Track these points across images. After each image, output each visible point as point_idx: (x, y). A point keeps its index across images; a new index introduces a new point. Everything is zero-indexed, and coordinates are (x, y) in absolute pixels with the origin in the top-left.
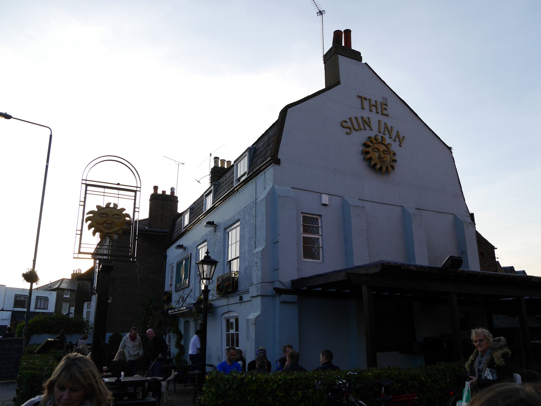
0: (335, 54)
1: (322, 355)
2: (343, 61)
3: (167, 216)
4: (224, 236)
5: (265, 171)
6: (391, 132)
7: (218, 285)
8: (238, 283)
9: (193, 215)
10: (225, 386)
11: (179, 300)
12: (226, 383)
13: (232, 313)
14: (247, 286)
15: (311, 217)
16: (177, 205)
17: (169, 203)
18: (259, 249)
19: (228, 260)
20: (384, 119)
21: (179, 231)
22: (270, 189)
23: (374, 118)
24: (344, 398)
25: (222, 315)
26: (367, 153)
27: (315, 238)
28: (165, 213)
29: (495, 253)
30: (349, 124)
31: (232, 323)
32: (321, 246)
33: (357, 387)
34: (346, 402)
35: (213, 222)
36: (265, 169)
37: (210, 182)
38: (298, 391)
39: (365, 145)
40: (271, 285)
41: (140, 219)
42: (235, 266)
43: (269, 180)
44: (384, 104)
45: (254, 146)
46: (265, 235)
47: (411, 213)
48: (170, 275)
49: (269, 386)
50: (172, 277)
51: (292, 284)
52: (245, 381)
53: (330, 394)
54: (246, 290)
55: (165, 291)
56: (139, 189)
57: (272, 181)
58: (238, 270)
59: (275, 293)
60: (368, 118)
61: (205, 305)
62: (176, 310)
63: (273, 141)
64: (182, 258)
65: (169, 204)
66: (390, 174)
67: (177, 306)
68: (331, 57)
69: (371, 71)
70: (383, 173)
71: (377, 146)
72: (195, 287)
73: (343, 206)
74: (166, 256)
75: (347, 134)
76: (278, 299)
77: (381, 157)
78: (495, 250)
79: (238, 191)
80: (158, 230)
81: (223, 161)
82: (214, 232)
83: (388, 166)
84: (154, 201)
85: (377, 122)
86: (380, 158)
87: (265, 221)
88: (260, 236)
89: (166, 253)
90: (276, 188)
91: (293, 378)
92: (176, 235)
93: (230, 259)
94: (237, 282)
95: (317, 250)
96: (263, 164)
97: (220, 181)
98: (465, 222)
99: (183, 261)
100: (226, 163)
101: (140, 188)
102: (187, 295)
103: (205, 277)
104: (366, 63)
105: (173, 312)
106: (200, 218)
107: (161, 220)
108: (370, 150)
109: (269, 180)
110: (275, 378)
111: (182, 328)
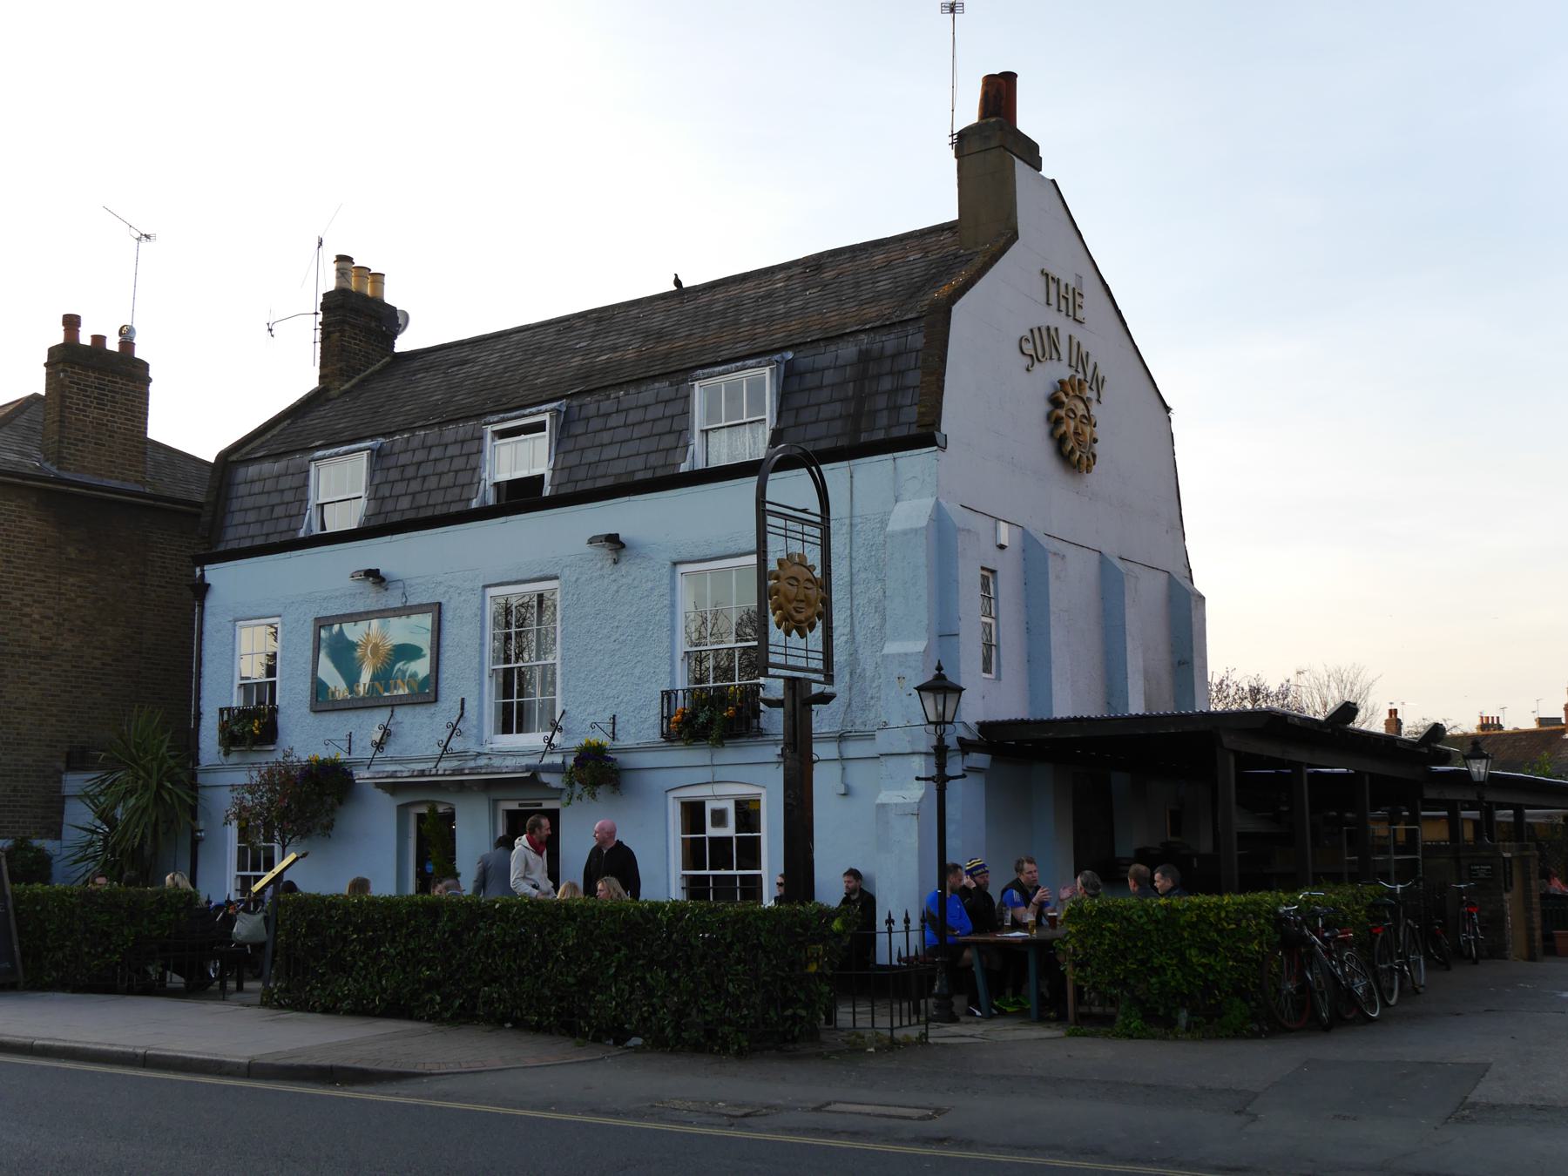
0: (1002, 149)
17: (123, 384)
28: (108, 421)
32: (994, 642)
65: (121, 388)
107: (96, 444)
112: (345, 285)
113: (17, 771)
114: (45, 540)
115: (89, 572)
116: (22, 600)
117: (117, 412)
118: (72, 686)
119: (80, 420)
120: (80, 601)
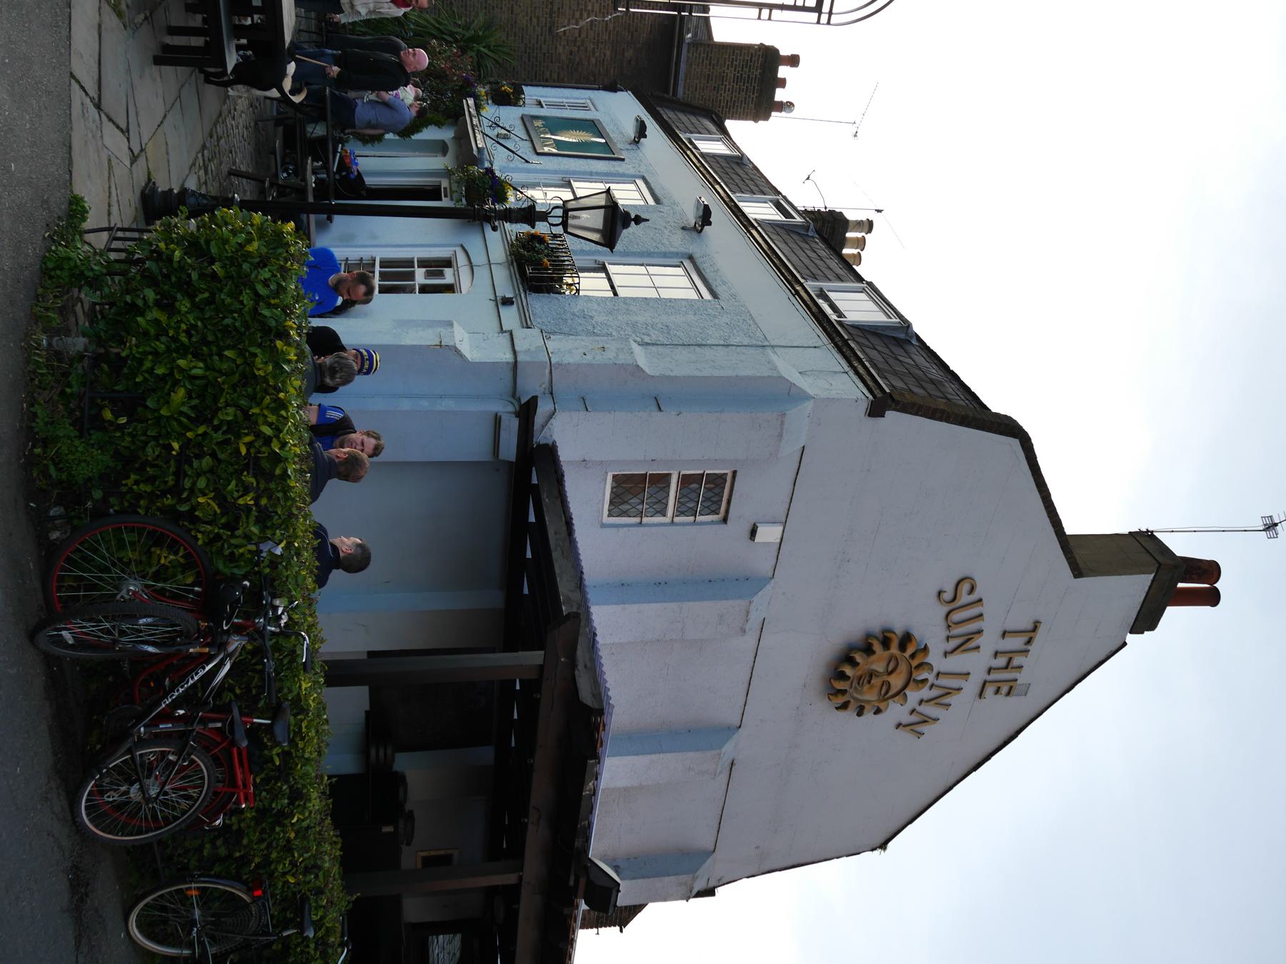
1: (359, 545)
2: (1137, 586)
3: (720, 92)
4: (672, 253)
5: (851, 373)
6: (936, 704)
7: (543, 238)
8: (549, 293)
9: (724, 164)
10: (266, 283)
11: (502, 128)
12: (273, 287)
13: (469, 277)
14: (539, 320)
15: (722, 497)
16: (746, 119)
17: (753, 98)
18: (641, 357)
19: (607, 264)
20: (971, 687)
21: (680, 125)
22: (803, 388)
23: (976, 663)
24: (236, 620)
25: (462, 246)
26: (886, 643)
27: (666, 505)
28: (726, 85)
29: (610, 926)
30: (964, 598)
31: (441, 274)
32: (645, 520)
33: (268, 661)
34: (225, 628)
35: (710, 224)
36: (857, 373)
37: (806, 210)
38: (252, 495)
39: (907, 639)
40: (545, 389)
41: (713, 22)
42: (591, 284)
43: (827, 386)
44: (1011, 687)
45: (915, 338)
46: (678, 375)
47: (723, 750)
48: (565, 100)
49: (266, 412)
50: (560, 106)
51: (546, 445)
52: (279, 344)
53: (246, 585)
54: (530, 317)
55: (523, 87)
56: (824, 18)
57: (824, 395)
58: (581, 293)
59: (524, 401)
60: (978, 648)
61: (493, 215)
62: (475, 121)
63: (930, 395)
64: (611, 135)
65: (749, 97)
66: (827, 699)
67: (485, 122)
68: (1148, 552)
69: (1103, 657)
70: (831, 683)
71: (903, 667)
72: (536, 171)
73: (747, 579)
74: (615, 91)
75: (940, 593)
76: (506, 409)
77: (873, 677)
78: (618, 928)
79: (794, 296)
80: (683, 66)
81: (861, 243)
82: (683, 225)
83: (848, 694)
84: (759, 55)
85: (965, 671)
86: (871, 676)
87: (717, 373)
88: (677, 361)
89: (622, 90)
90: (805, 405)
91: (288, 482)
92: (670, 118)
93: (612, 269)
94: (550, 290)
95: (634, 510)
96: (871, 369)
97: (816, 242)
98: (694, 877)
99: (603, 137)
100: (855, 251)
101: (829, 23)
102: (514, 150)
103: (570, 213)
104: (1125, 644)
105: (469, 111)
106: (717, 187)
107: (709, 75)
108: (894, 650)
109: (827, 386)
110: (287, 430)
111: (430, 134)
112: (851, 226)
113: (466, 6)
114: (636, 31)
115: (615, 68)
116: (592, 11)
117: (732, 93)
118: (529, 53)
119: (725, 63)
120: (593, 60)
